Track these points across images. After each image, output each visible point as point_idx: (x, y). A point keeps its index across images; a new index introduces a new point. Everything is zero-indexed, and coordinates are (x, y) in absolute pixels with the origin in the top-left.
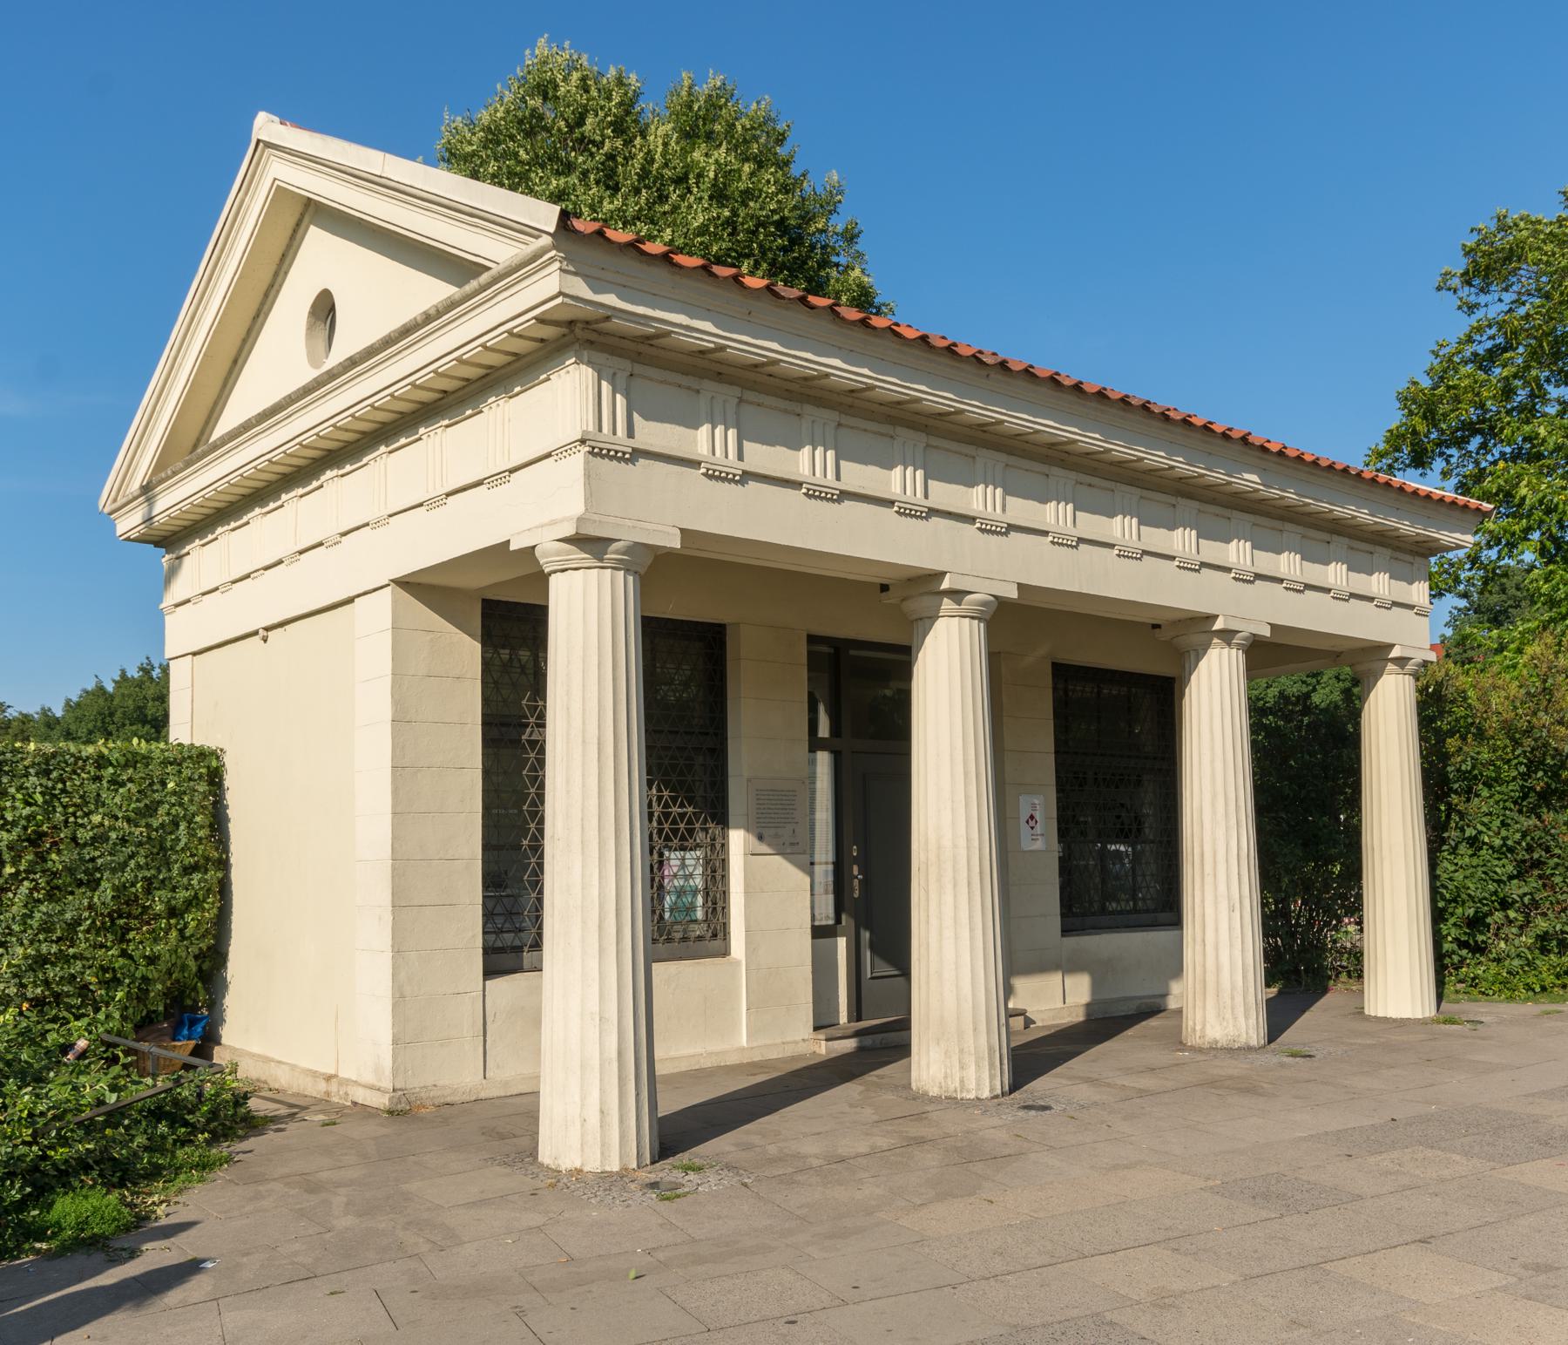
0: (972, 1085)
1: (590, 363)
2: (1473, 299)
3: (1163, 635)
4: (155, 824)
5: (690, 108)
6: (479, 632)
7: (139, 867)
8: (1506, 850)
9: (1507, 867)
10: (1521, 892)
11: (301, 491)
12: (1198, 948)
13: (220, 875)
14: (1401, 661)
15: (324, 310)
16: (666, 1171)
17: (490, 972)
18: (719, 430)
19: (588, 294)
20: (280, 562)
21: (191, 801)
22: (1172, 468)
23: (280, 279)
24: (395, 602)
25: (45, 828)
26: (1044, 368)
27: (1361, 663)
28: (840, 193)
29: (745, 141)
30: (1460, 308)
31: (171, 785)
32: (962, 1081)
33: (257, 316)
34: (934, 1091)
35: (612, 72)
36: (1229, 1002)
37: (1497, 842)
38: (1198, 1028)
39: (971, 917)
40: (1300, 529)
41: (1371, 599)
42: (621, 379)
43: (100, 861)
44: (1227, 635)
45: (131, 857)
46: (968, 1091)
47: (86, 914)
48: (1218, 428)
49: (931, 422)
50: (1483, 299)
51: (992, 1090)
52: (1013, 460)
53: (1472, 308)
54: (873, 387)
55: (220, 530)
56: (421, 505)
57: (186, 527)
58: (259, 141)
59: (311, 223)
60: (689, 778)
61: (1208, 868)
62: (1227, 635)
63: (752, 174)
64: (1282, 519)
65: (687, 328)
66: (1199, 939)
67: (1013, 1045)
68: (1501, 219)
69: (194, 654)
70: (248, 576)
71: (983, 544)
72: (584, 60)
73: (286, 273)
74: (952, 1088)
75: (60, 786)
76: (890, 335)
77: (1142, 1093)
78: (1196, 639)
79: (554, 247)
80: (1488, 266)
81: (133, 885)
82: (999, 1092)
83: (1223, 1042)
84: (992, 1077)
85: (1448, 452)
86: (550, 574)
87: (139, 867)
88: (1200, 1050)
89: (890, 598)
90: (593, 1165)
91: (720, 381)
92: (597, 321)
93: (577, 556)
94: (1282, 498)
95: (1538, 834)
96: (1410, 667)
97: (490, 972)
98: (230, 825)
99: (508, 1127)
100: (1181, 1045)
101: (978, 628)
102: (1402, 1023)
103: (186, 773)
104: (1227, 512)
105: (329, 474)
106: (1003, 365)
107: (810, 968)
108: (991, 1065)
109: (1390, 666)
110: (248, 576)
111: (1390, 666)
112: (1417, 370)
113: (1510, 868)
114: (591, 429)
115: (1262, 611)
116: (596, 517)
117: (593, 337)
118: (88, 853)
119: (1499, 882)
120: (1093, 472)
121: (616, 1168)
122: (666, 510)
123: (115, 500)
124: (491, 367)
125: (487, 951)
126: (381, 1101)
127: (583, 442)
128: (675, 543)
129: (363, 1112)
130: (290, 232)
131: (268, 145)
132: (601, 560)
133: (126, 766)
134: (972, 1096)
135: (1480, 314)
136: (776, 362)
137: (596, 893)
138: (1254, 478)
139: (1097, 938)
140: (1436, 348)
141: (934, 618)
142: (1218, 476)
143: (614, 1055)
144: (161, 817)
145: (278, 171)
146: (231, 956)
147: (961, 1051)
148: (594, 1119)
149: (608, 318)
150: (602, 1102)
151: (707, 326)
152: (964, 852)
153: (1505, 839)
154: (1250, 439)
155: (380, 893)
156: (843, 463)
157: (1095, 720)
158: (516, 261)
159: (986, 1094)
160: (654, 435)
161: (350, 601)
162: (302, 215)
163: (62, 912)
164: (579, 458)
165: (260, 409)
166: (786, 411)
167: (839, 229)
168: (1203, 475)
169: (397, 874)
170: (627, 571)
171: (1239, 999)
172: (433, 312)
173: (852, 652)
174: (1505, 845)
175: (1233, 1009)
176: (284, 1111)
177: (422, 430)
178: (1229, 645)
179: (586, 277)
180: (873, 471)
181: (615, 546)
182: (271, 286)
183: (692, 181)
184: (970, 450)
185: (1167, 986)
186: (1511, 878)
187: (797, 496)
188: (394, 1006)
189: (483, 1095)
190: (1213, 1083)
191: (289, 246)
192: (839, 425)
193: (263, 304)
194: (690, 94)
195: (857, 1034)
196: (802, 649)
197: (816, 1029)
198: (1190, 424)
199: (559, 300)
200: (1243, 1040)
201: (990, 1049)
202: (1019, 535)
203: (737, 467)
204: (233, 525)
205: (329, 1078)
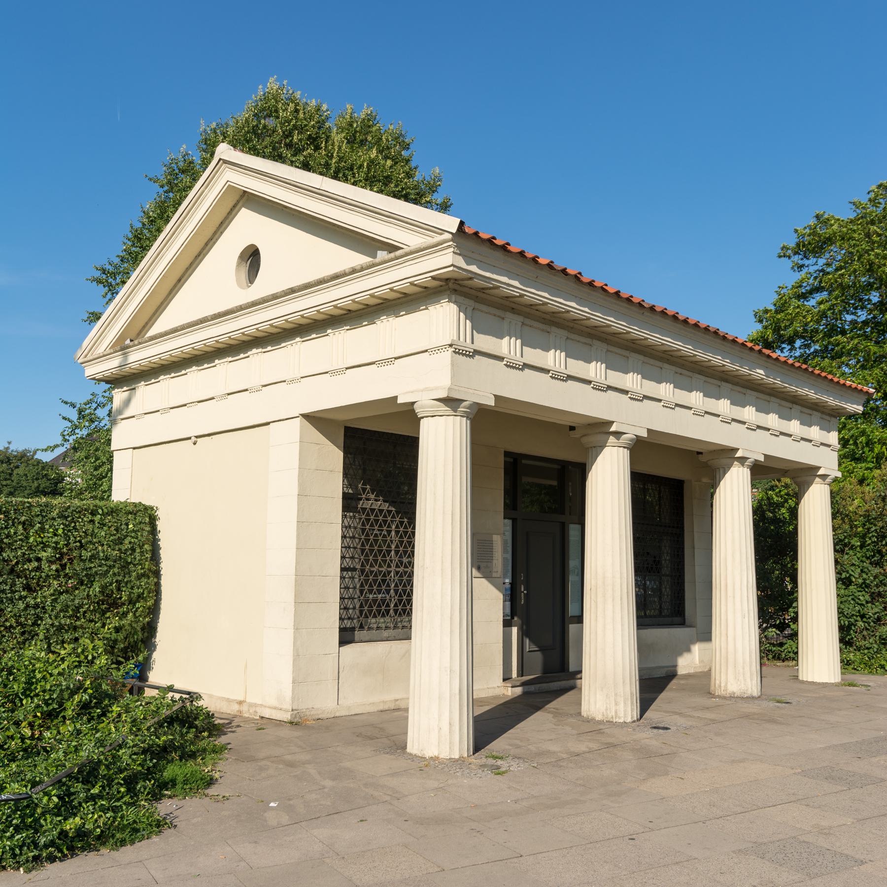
0: (622, 714)
1: (455, 302)
2: (801, 262)
3: (702, 458)
4: (123, 549)
5: (351, 125)
6: (342, 445)
7: (114, 574)
8: (865, 586)
9: (864, 597)
10: (874, 611)
11: (230, 359)
12: (723, 639)
13: (156, 580)
14: (824, 477)
15: (252, 258)
17: (343, 642)
19: (464, 265)
20: (213, 398)
21: (142, 535)
22: (724, 365)
23: (217, 236)
24: (301, 427)
25: (65, 550)
26: (671, 310)
27: (803, 475)
28: (440, 180)
29: (388, 148)
30: (792, 268)
31: (131, 526)
32: (616, 712)
33: (199, 255)
34: (599, 717)
35: (313, 103)
36: (741, 670)
37: (860, 581)
38: (723, 685)
40: (778, 401)
41: (810, 441)
42: (470, 309)
43: (94, 570)
44: (742, 460)
45: (110, 567)
46: (620, 718)
47: (85, 601)
49: (609, 337)
50: (806, 262)
51: (632, 718)
52: (647, 359)
53: (801, 267)
54: (589, 319)
55: (162, 377)
56: (327, 373)
57: (134, 374)
58: (220, 159)
59: (243, 206)
60: (859, 555)
61: (730, 593)
62: (742, 460)
63: (391, 167)
64: (770, 394)
66: (724, 632)
68: (818, 217)
69: (134, 448)
70: (185, 405)
72: (298, 94)
73: (222, 233)
74: (610, 716)
75: (73, 525)
76: (601, 291)
77: (713, 721)
78: (724, 461)
79: (452, 240)
80: (812, 245)
81: (111, 584)
83: (738, 694)
85: (783, 346)
86: (422, 418)
87: (114, 574)
88: (725, 698)
89: (575, 434)
90: (445, 754)
91: (514, 313)
92: (463, 280)
93: (443, 408)
94: (774, 383)
95: (881, 578)
96: (828, 480)
97: (343, 642)
98: (161, 551)
99: (385, 731)
100: (710, 694)
101: (627, 453)
102: (824, 685)
103: (138, 519)
104: (744, 390)
105: (254, 351)
107: (501, 645)
108: (632, 703)
109: (817, 479)
110: (185, 405)
111: (817, 479)
112: (768, 302)
113: (868, 597)
114: (455, 338)
115: (756, 447)
116: (456, 388)
117: (457, 287)
118: (88, 565)
119: (861, 605)
120: (682, 366)
121: (457, 757)
122: (490, 384)
123: (86, 356)
124: (386, 299)
125: (342, 630)
126: (287, 717)
127: (451, 345)
128: (491, 402)
129: (280, 723)
130: (228, 210)
131: (225, 162)
132: (455, 411)
133: (108, 514)
134: (621, 721)
135: (805, 270)
136: (545, 304)
137: (449, 598)
138: (762, 372)
139: (645, 631)
140: (777, 289)
141: (602, 447)
142: (745, 370)
143: (457, 692)
144: (126, 545)
145: (230, 176)
146: (158, 629)
147: (616, 695)
148: (446, 728)
149: (471, 279)
150: (451, 719)
151: (516, 283)
152: (619, 581)
153: (864, 579)
155: (288, 595)
158: (424, 245)
159: (629, 720)
160: (485, 342)
161: (268, 424)
162: (238, 202)
163: (73, 600)
164: (449, 353)
165: (216, 312)
166: (543, 330)
167: (439, 201)
168: (738, 370)
169: (298, 584)
170: (467, 417)
171: (747, 669)
172: (359, 268)
173: (524, 461)
174: (864, 583)
175: (744, 674)
176: (227, 721)
177: (329, 331)
178: (743, 465)
181: (464, 404)
182: (211, 239)
183: (355, 171)
184: (626, 353)
185: (676, 661)
186: (867, 602)
187: (547, 377)
188: (294, 660)
189: (337, 714)
190: (747, 716)
191: (226, 218)
192: (608, 351)
193: (203, 249)
194: (351, 117)
195: (523, 684)
196: (502, 459)
197: (504, 680)
199: (451, 268)
201: (632, 694)
203: (520, 361)
204: (173, 375)
205: (240, 703)
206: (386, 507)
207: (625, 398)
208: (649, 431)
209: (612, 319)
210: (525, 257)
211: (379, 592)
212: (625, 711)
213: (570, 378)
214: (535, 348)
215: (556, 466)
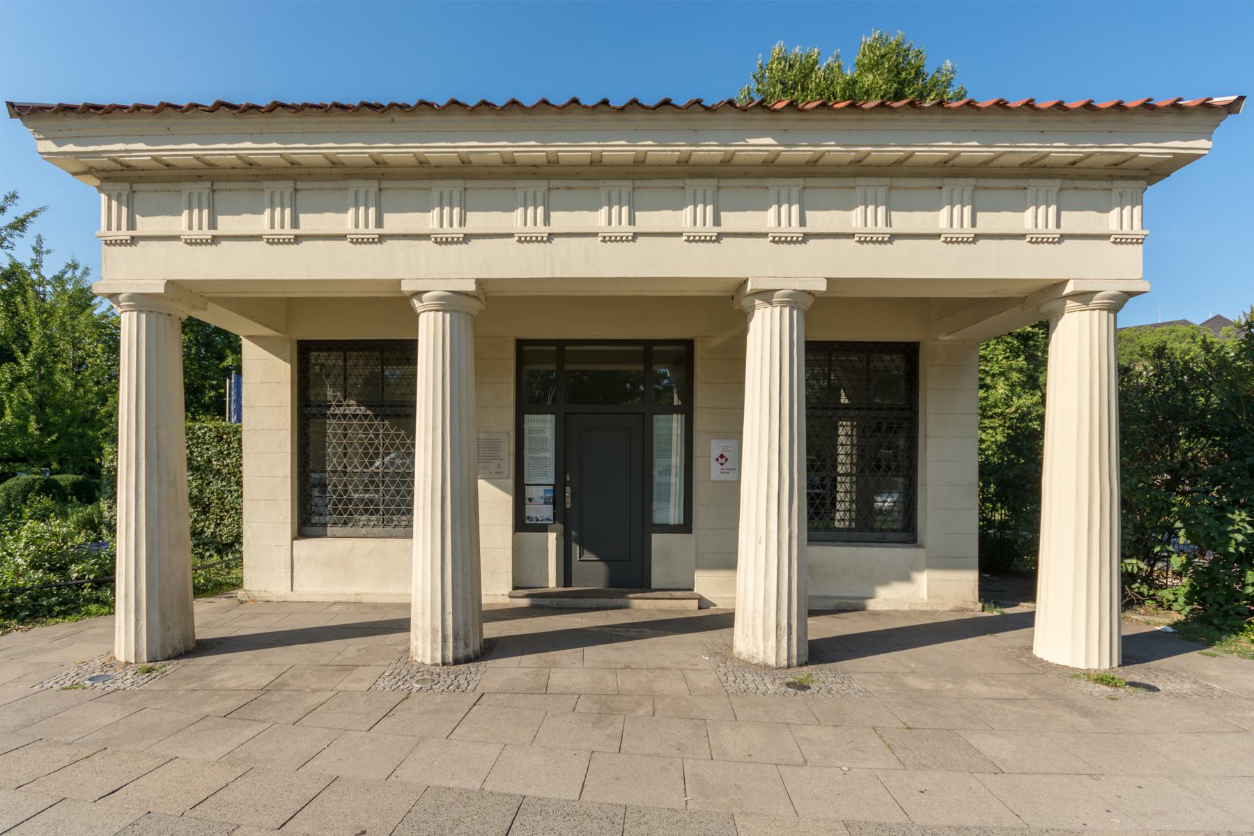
16: (1137, 673)
18: (278, 211)
39: (424, 532)
48: (1073, 103)
62: (1083, 297)
65: (126, 151)
67: (1124, 633)
71: (781, 256)
82: (439, 661)
84: (433, 650)
96: (1096, 301)
106: (1119, 107)
107: (510, 551)
108: (434, 641)
111: (1070, 304)
128: (822, 287)
151: (141, 146)
154: (1038, 104)
156: (808, 213)
157: (870, 383)
166: (251, 190)
173: (655, 348)
175: (753, 629)
178: (771, 304)
179: (53, 139)
180: (1092, 215)
192: (976, 188)
198: (1182, 108)
200: (760, 658)
201: (433, 630)
202: (901, 241)
206: (362, 410)
207: (938, 243)
208: (479, 282)
209: (533, 143)
210: (1066, 109)
211: (366, 491)
212: (424, 649)
213: (894, 237)
214: (239, 214)
215: (642, 348)
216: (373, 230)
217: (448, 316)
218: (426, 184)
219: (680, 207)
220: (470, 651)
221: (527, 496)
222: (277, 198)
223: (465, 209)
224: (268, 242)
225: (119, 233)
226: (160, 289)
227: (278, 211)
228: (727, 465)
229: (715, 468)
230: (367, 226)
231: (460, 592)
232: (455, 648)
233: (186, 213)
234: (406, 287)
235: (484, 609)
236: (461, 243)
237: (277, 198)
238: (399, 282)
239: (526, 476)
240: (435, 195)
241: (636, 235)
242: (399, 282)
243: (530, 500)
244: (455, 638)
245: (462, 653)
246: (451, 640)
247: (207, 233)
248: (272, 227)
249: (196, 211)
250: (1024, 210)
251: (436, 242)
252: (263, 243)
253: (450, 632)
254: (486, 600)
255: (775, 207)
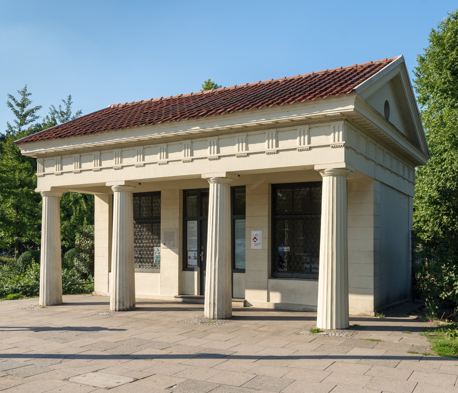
216: (245, 152)
217: (335, 178)
218: (112, 151)
219: (328, 134)
220: (125, 307)
221: (189, 256)
222: (270, 135)
223: (122, 158)
224: (267, 154)
225: (304, 146)
226: (224, 176)
227: (302, 137)
228: (257, 242)
229: (253, 242)
230: (339, 141)
231: (121, 287)
232: (119, 306)
233: (267, 141)
234: (316, 168)
235: (350, 317)
236: (308, 150)
237: (270, 135)
238: (313, 166)
239: (188, 246)
240: (208, 143)
241: (168, 162)
242: (313, 166)
243: (190, 257)
244: (119, 302)
245: (121, 308)
246: (118, 303)
247: (216, 155)
248: (300, 145)
249: (186, 150)
250: (330, 135)
251: (237, 157)
252: (113, 170)
253: (118, 300)
254: (350, 313)
255: (184, 150)
